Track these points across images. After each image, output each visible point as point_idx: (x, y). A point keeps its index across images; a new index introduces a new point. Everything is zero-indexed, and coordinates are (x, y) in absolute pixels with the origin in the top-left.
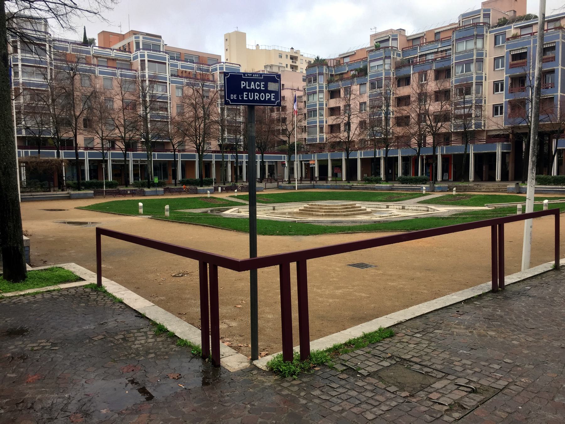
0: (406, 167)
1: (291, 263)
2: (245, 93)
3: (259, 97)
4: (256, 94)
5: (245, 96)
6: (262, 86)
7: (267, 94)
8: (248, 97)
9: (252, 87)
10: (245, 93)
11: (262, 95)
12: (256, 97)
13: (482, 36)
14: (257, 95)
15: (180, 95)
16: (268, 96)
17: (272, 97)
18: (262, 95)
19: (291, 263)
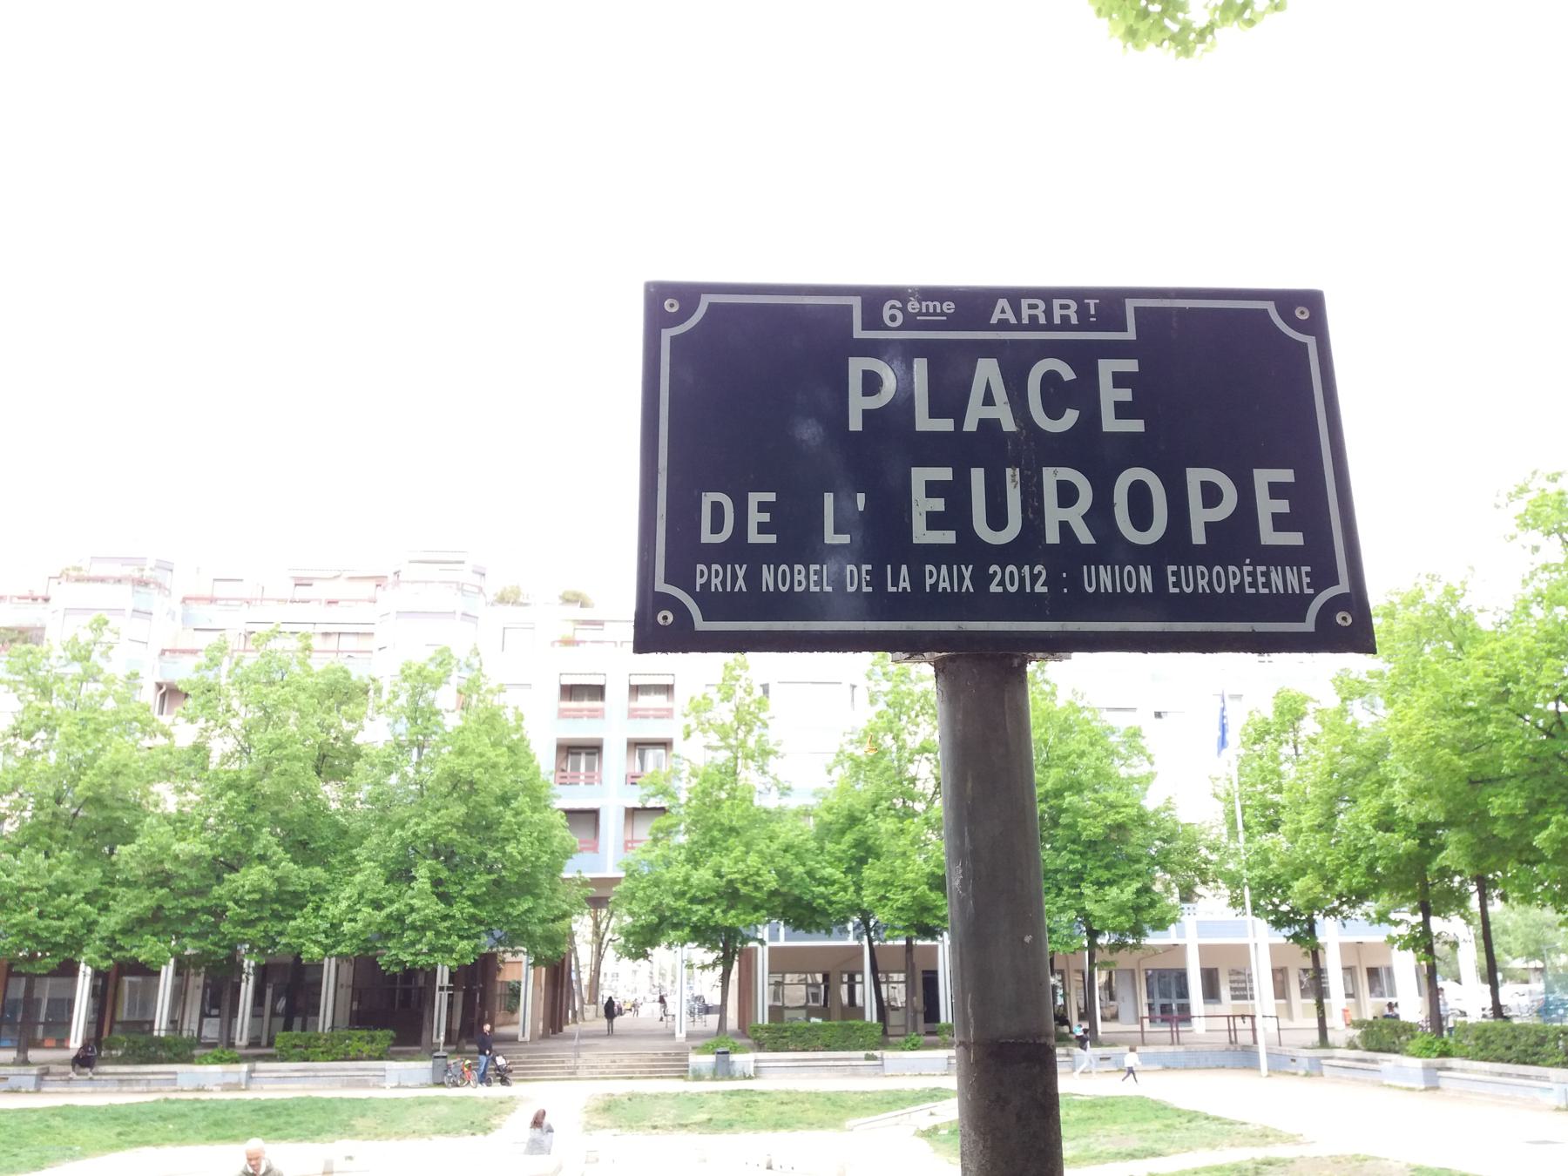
0: (554, 998)
1: (851, 359)
2: (921, 476)
3: (1100, 515)
4: (1051, 477)
5: (923, 505)
6: (1110, 396)
7: (1195, 477)
8: (955, 515)
9: (902, 584)
10: (921, 476)
11: (1139, 493)
12: (1054, 515)
13: (689, 1036)
14: (1067, 495)
15: (82, 641)
16: (1211, 495)
17: (1267, 508)
18: (1139, 493)
19: (851, 359)
